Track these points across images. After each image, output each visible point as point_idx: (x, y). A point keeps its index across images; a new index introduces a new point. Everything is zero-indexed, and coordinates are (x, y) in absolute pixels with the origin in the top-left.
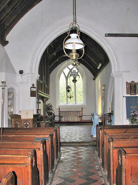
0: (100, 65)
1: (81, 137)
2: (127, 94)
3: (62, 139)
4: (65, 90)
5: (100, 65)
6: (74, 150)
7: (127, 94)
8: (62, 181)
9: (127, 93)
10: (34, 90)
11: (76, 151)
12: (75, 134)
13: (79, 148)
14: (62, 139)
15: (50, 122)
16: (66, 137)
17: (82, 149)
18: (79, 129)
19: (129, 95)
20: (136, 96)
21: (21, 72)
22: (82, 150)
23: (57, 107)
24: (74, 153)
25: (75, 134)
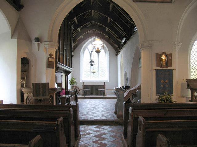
0: (124, 39)
1: (104, 113)
2: (33, 83)
3: (84, 115)
4: (89, 64)
5: (124, 39)
6: (96, 131)
7: (33, 83)
8: (85, 144)
9: (157, 66)
10: (54, 60)
11: (98, 133)
12: (98, 109)
13: (102, 128)
14: (84, 115)
15: (71, 96)
16: (88, 113)
17: (105, 129)
18: (102, 103)
19: (159, 68)
20: (167, 69)
21: (38, 40)
22: (106, 131)
23: (81, 81)
24: (96, 136)
25: (98, 109)
